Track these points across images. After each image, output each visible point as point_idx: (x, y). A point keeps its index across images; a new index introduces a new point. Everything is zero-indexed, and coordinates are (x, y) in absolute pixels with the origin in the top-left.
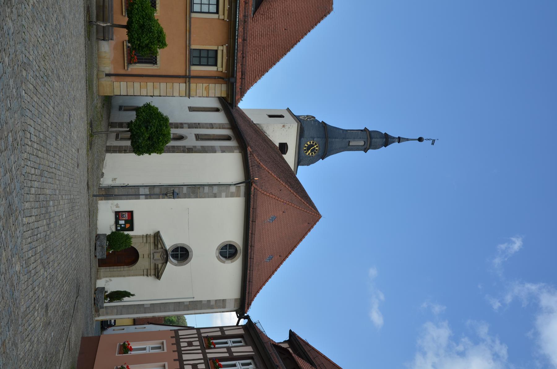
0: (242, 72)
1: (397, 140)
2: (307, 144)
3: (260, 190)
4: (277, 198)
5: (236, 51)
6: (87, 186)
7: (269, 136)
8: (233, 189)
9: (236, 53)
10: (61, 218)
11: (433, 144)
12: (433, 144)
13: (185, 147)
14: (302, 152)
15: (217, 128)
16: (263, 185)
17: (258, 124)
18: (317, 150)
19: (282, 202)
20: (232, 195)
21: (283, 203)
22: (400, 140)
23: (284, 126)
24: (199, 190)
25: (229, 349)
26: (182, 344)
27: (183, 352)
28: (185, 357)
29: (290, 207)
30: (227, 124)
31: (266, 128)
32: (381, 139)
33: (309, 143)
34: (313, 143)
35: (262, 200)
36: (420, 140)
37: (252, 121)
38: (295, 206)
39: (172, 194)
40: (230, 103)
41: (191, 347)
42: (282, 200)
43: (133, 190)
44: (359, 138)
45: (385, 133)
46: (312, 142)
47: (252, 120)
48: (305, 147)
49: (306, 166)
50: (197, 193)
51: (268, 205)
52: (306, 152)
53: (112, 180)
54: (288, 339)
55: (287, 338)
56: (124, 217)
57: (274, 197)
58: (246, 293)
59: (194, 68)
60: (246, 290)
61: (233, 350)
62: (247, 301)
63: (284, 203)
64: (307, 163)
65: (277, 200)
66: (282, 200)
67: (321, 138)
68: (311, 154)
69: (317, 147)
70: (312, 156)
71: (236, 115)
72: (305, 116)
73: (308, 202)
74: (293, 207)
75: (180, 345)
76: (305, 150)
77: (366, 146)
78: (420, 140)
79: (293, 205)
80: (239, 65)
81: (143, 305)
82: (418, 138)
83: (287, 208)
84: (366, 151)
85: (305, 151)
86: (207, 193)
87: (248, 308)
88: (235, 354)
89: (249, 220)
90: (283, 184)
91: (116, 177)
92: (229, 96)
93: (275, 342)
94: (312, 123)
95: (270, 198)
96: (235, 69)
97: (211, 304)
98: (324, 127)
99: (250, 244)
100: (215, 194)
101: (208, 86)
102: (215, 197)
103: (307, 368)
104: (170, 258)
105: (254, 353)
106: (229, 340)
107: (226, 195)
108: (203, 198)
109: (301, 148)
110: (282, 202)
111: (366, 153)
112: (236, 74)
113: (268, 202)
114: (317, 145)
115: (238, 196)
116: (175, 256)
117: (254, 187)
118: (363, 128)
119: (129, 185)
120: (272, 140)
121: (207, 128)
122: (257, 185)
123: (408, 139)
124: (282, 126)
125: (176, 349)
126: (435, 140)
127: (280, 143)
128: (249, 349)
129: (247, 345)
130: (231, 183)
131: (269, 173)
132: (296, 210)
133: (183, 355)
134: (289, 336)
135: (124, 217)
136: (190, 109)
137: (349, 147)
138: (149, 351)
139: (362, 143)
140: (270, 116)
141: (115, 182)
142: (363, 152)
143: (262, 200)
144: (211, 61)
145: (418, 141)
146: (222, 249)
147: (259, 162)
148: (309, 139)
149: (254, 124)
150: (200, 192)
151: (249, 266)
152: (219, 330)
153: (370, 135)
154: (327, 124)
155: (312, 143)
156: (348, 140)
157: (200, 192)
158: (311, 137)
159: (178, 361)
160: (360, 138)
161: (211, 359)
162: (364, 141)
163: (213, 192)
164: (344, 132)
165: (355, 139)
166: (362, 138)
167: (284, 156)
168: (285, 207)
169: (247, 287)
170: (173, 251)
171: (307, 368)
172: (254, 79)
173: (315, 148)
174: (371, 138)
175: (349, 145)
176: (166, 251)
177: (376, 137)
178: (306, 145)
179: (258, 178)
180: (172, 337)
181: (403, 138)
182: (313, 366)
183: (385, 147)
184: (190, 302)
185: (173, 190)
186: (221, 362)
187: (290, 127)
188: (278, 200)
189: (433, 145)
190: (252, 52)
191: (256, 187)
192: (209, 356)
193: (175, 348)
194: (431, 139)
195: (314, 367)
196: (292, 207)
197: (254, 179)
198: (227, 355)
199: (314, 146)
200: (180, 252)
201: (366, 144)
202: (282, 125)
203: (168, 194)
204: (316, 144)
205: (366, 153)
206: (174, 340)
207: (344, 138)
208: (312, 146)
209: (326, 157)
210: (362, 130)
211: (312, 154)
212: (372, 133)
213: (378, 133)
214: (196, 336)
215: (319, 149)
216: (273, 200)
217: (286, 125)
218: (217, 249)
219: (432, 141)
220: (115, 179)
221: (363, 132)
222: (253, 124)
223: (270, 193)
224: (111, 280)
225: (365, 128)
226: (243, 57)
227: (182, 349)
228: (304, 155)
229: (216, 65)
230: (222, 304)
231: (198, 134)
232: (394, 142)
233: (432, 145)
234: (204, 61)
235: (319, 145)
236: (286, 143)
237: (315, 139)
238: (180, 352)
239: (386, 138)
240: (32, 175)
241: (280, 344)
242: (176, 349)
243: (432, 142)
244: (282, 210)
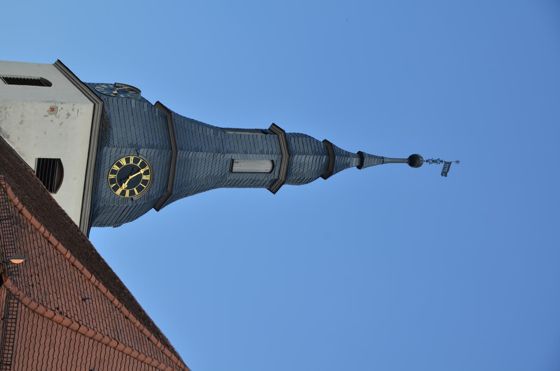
1: (356, 161)
2: (119, 165)
3: (26, 300)
4: (75, 326)
7: (8, 137)
11: (444, 173)
12: (444, 173)
14: (105, 187)
16: (35, 284)
18: (145, 182)
19: (91, 338)
21: (91, 341)
23: (52, 109)
29: (73, 337)
32: (316, 157)
33: (123, 162)
34: (136, 160)
35: (29, 334)
36: (414, 161)
38: (128, 350)
42: (91, 333)
44: (258, 151)
46: (132, 158)
48: (114, 172)
49: (111, 228)
51: (47, 349)
52: (116, 188)
57: (67, 322)
63: (96, 342)
64: (114, 220)
65: (74, 333)
66: (121, 344)
67: (157, 148)
68: (128, 192)
69: (146, 173)
70: (132, 199)
72: (112, 86)
74: (121, 354)
76: (112, 181)
77: (276, 173)
78: (414, 161)
79: (121, 347)
83: (102, 357)
90: (89, 280)
94: (133, 106)
95: (55, 324)
98: (166, 118)
109: (101, 177)
110: (91, 338)
111: (274, 193)
113: (48, 340)
114: (147, 168)
117: (8, 290)
120: (17, 151)
122: (15, 283)
123: (383, 158)
124: (48, 108)
126: (450, 163)
127: (39, 160)
131: (49, 242)
132: (136, 364)
137: (232, 177)
139: (266, 166)
140: (10, 81)
142: (264, 192)
143: (29, 334)
145: (406, 165)
147: (20, 206)
148: (124, 150)
153: (287, 144)
155: (131, 162)
156: (229, 156)
158: (131, 146)
160: (262, 152)
162: (272, 161)
164: (219, 135)
165: (248, 155)
166: (268, 153)
167: (54, 196)
168: (98, 355)
173: (141, 175)
174: (290, 153)
175: (231, 170)
177: (302, 150)
178: (116, 168)
179: (21, 261)
181: (371, 156)
183: (325, 178)
187: (71, 112)
188: (77, 331)
189: (446, 176)
191: (14, 289)
194: (442, 161)
196: (117, 352)
197: (8, 262)
199: (139, 171)
201: (277, 168)
202: (48, 106)
204: (143, 165)
205: (274, 193)
207: (218, 152)
208: (134, 169)
210: (264, 132)
211: (132, 193)
212: (292, 139)
213: (308, 139)
215: (152, 178)
216: (63, 334)
217: (60, 106)
219: (442, 165)
221: (268, 136)
223: (53, 309)
228: (108, 196)
232: (347, 166)
233: (442, 175)
235: (152, 167)
236: (59, 160)
237: (142, 150)
239: (328, 155)
243: (444, 168)
244: (88, 363)
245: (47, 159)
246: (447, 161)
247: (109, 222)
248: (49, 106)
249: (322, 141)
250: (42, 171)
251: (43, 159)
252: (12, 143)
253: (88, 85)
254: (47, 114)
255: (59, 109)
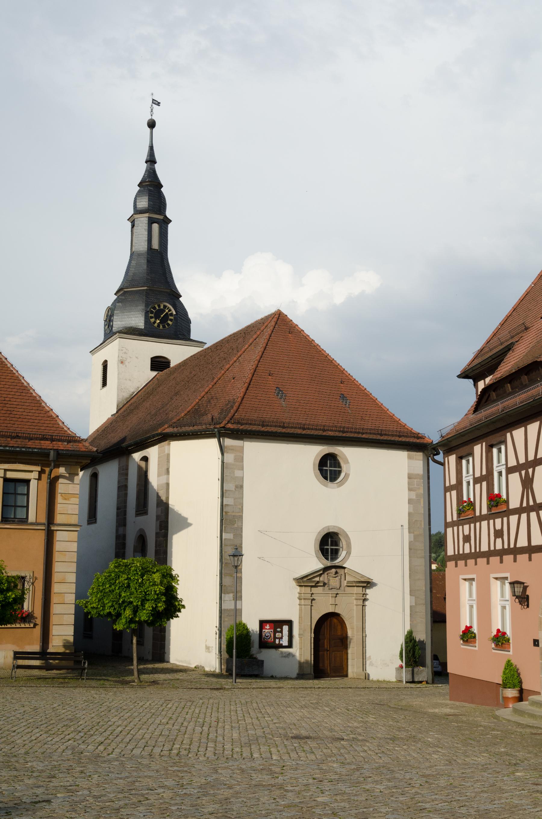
0: (41, 439)
5: (7, 448)
6: (219, 691)
7: (138, 388)
8: (229, 458)
9: (10, 449)
10: (271, 723)
11: (158, 104)
12: (158, 104)
13: (157, 534)
15: (127, 479)
17: (117, 407)
20: (240, 459)
22: (151, 160)
24: (229, 512)
25: (477, 481)
26: (467, 551)
27: (478, 550)
28: (484, 548)
30: (119, 462)
31: (124, 392)
36: (152, 125)
37: (112, 415)
39: (236, 559)
40: (91, 460)
41: (463, 541)
43: (226, 619)
45: (139, 185)
46: (151, 315)
47: (110, 416)
50: (234, 516)
53: (209, 652)
54: (471, 381)
55: (470, 382)
56: (269, 634)
58: (398, 441)
59: (32, 518)
60: (394, 441)
61: (478, 475)
62: (412, 440)
71: (104, 444)
73: (254, 332)
75: (467, 553)
78: (152, 125)
80: (30, 444)
81: (411, 607)
82: (148, 130)
84: (167, 221)
85: (165, 327)
86: (234, 499)
87: (423, 438)
88: (484, 473)
89: (280, 433)
91: (205, 646)
92: (79, 461)
93: (469, 411)
96: (36, 450)
97: (414, 497)
99: (320, 433)
100: (237, 487)
101: (61, 495)
102: (242, 487)
103: (541, 330)
104: (337, 562)
105: (484, 444)
106: (464, 479)
107: (239, 470)
108: (242, 507)
112: (44, 449)
115: (241, 450)
116: (335, 553)
118: (129, 224)
119: (218, 626)
121: (126, 495)
124: (121, 365)
125: (473, 561)
126: (153, 100)
127: (151, 370)
128: (477, 449)
129: (471, 454)
130: (220, 460)
133: (482, 550)
134: (467, 380)
135: (269, 634)
136: (92, 522)
138: (474, 600)
140: (104, 384)
141: (212, 647)
144: (21, 489)
145: (154, 129)
146: (326, 478)
149: (117, 412)
150: (233, 512)
151: (356, 435)
152: (449, 493)
154: (119, 285)
155: (153, 315)
157: (233, 512)
159: (489, 559)
161: (489, 508)
163: (234, 490)
167: (172, 365)
169: (389, 438)
170: (327, 559)
171: (541, 330)
172: (52, 419)
176: (326, 569)
180: (456, 565)
182: (511, 349)
184: (409, 532)
185: (229, 556)
186: (529, 474)
189: (159, 103)
190: (8, 422)
192: (485, 511)
193: (471, 562)
195: (513, 347)
198: (484, 484)
200: (328, 546)
203: (236, 565)
206: (461, 563)
209: (177, 291)
210: (133, 226)
214: (455, 528)
218: (326, 486)
219: (154, 105)
220: (208, 648)
222: (117, 415)
224: (370, 657)
225: (128, 220)
226: (17, 437)
227: (473, 551)
229: (27, 482)
230: (415, 480)
231: (136, 511)
234: (21, 500)
236: (152, 358)
238: (476, 555)
240: (215, 750)
241: (479, 393)
242: (473, 561)
243: (155, 104)
245: (151, 365)
246: (152, 102)
247: (188, 327)
248: (370, 657)
249: (139, 188)
250: (158, 368)
251: (151, 367)
252: (142, 385)
253: (106, 340)
254: (125, 365)
255: (121, 358)
